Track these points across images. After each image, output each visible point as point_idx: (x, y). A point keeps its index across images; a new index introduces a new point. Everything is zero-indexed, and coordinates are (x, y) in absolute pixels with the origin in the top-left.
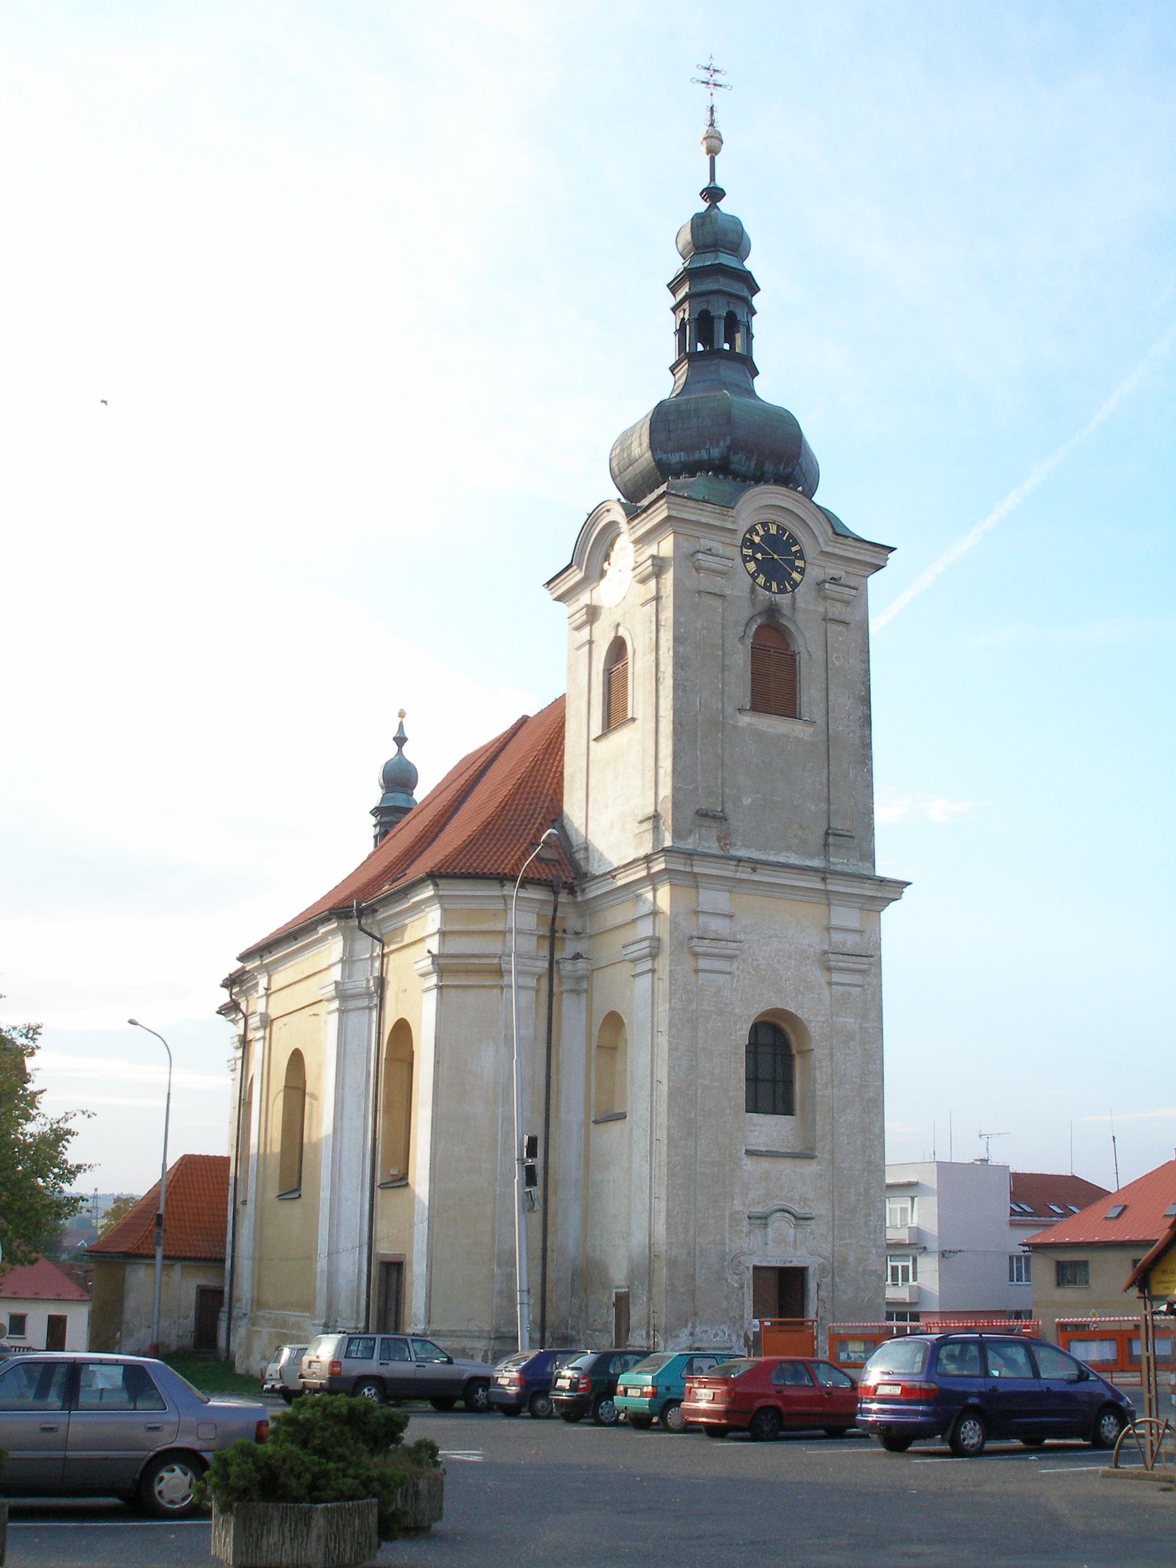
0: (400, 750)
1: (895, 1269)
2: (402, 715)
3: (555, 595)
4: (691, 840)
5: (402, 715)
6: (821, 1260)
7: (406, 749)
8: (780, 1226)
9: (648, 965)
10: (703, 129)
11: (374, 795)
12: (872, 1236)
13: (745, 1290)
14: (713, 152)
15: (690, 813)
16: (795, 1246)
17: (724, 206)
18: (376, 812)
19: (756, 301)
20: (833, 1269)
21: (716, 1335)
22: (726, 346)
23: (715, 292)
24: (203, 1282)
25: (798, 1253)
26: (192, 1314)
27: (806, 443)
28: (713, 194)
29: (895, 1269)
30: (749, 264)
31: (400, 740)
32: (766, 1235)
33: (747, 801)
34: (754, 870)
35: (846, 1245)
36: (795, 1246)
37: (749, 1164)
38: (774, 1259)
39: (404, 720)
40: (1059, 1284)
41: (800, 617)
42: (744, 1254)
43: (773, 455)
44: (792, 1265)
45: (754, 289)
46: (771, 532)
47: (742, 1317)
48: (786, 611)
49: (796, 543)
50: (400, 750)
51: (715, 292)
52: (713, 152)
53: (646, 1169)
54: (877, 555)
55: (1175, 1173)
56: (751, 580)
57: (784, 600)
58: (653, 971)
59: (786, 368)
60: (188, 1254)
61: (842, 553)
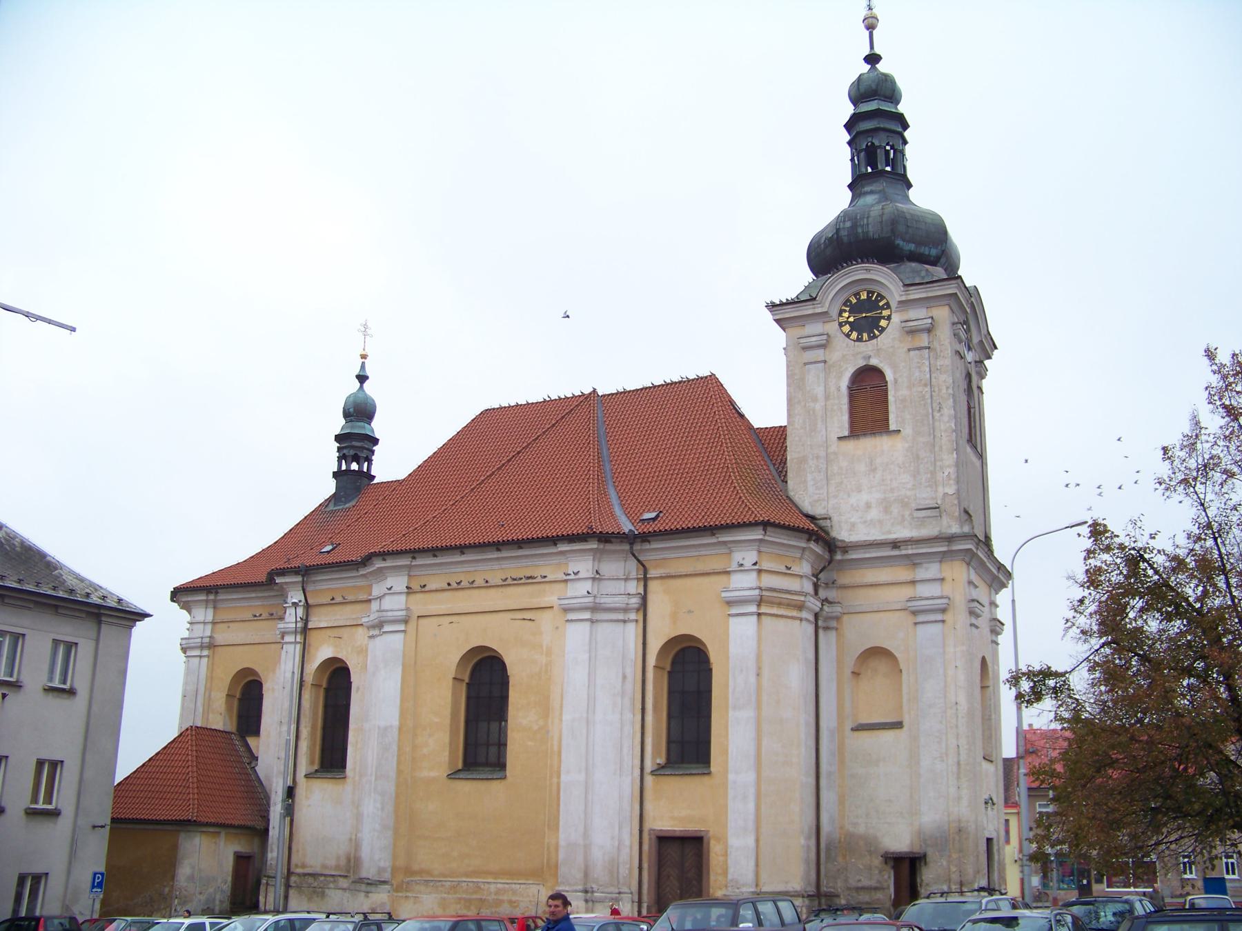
0: (361, 386)
2: (364, 357)
5: (364, 357)
7: (366, 385)
9: (402, 627)
10: (864, 12)
11: (338, 424)
14: (871, 28)
17: (881, 67)
18: (338, 438)
19: (907, 134)
22: (888, 169)
23: (876, 128)
26: (230, 879)
27: (952, 243)
28: (872, 59)
30: (901, 108)
31: (362, 378)
34: (414, 558)
43: (922, 249)
45: (905, 126)
50: (361, 386)
51: (876, 128)
52: (871, 28)
53: (750, 777)
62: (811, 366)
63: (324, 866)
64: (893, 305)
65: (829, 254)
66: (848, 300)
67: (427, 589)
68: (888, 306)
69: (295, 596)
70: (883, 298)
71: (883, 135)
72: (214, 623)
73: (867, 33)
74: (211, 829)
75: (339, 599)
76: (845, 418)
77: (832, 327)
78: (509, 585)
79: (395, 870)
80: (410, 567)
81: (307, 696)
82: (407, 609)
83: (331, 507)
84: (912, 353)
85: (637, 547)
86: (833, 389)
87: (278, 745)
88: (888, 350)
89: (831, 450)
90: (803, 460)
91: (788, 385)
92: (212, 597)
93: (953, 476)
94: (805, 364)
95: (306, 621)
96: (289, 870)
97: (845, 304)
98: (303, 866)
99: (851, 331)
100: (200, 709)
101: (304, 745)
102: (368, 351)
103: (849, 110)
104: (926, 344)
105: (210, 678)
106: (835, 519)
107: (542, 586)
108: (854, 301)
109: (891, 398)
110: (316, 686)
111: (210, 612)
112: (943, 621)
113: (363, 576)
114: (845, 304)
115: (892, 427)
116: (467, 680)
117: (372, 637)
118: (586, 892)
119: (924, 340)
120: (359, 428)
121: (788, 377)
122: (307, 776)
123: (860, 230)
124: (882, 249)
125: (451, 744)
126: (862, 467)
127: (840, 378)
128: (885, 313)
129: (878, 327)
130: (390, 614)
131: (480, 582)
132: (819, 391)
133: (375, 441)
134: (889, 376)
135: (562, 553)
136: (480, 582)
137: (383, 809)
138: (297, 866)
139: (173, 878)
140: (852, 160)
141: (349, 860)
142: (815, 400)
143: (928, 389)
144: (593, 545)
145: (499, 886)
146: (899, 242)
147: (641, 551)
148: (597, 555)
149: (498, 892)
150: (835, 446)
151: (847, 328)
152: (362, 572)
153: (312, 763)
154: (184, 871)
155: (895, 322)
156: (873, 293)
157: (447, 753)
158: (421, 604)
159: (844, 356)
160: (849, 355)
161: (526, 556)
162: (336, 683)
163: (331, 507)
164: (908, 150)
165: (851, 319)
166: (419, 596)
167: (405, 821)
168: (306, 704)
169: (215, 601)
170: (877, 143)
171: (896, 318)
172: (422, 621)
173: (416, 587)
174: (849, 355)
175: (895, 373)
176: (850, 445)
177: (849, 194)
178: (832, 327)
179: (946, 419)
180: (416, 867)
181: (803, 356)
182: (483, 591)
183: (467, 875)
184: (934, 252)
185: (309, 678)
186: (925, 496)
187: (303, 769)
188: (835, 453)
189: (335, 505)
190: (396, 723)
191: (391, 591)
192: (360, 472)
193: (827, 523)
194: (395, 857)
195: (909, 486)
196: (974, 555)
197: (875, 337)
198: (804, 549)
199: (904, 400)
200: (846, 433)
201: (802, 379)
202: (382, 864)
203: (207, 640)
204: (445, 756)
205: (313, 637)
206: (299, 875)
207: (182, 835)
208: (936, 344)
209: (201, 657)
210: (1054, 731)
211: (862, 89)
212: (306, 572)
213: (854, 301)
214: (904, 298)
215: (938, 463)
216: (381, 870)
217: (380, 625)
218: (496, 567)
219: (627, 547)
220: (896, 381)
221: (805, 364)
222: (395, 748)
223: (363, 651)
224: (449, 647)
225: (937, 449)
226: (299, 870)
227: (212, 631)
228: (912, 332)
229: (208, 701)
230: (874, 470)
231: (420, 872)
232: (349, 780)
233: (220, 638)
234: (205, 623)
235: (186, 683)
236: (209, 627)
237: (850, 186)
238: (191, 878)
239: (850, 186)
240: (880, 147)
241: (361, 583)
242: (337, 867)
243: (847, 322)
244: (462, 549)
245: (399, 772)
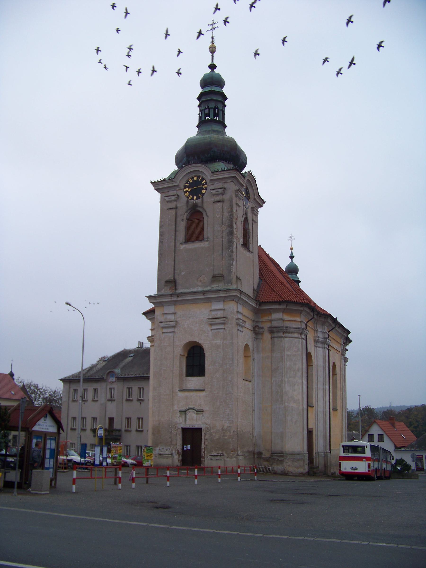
2: (292, 249)
3: (156, 188)
4: (163, 291)
5: (292, 249)
6: (206, 426)
8: (191, 415)
10: (210, 44)
12: (227, 417)
13: (178, 435)
15: (163, 282)
16: (197, 421)
17: (216, 71)
19: (226, 103)
20: (208, 429)
21: (167, 450)
23: (212, 97)
25: (198, 423)
28: (213, 67)
31: (292, 257)
32: (186, 417)
33: (183, 273)
35: (216, 420)
36: (197, 421)
37: (180, 394)
38: (189, 424)
40: (378, 435)
41: (205, 206)
42: (177, 424)
43: (234, 157)
44: (195, 427)
46: (195, 179)
47: (176, 444)
48: (200, 205)
49: (185, 186)
51: (212, 97)
54: (158, 186)
55: (425, 409)
56: (187, 199)
57: (199, 201)
59: (236, 128)
61: (217, 178)
64: (208, 182)
65: (190, 155)
68: (206, 183)
99: (189, 195)
102: (293, 247)
103: (200, 90)
108: (191, 181)
112: (224, 329)
128: (205, 187)
129: (201, 193)
140: (199, 114)
151: (187, 194)
164: (226, 110)
177: (197, 129)
196: (240, 298)
198: (302, 310)
210: (104, 366)
213: (191, 181)
237: (197, 126)
239: (197, 126)
243: (187, 191)
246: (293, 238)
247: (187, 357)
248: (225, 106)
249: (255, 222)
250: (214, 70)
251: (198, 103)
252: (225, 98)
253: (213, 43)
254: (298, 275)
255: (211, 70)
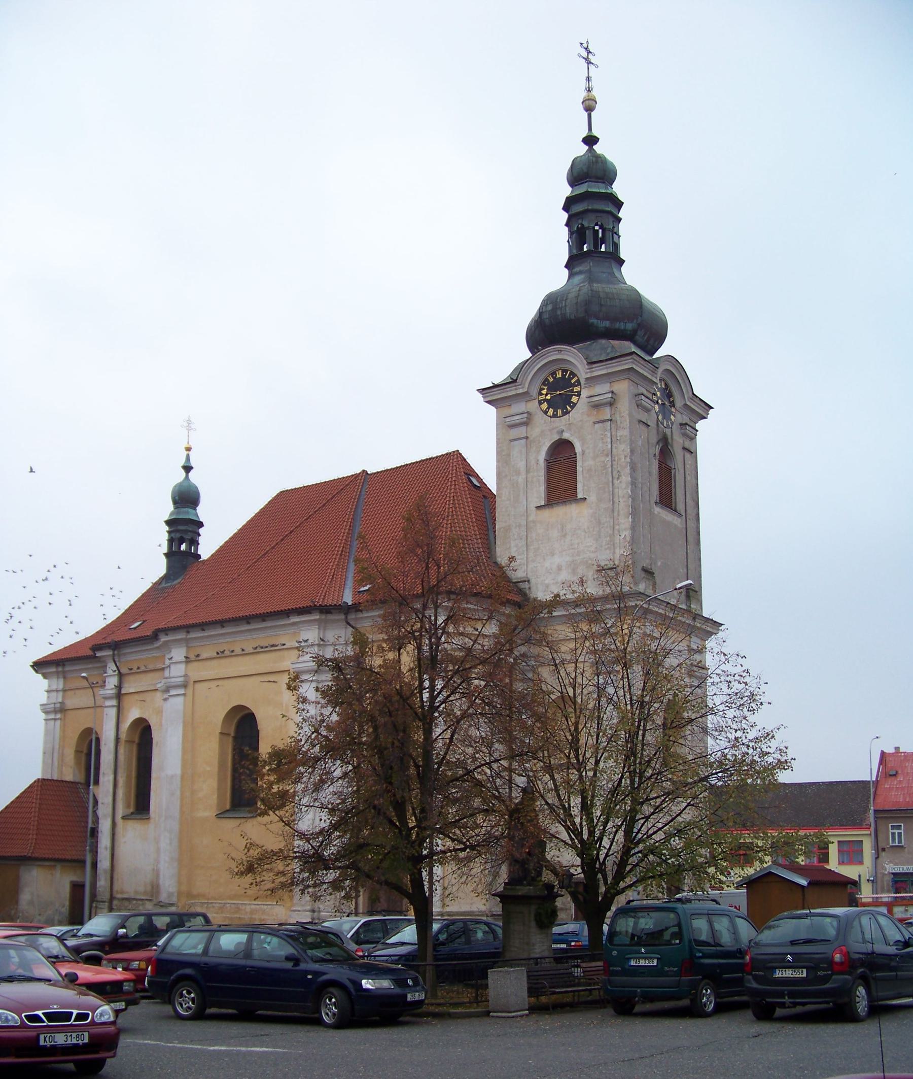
0: (187, 476)
1: (893, 834)
3: (488, 399)
7: (191, 474)
9: (182, 691)
10: (583, 94)
11: (167, 509)
18: (169, 523)
19: (621, 215)
23: (592, 205)
24: (75, 878)
26: (67, 903)
28: (590, 140)
29: (893, 834)
31: (188, 469)
34: (188, 632)
39: (190, 453)
43: (641, 328)
50: (187, 476)
51: (592, 205)
54: (493, 394)
58: (184, 695)
59: (646, 266)
60: (47, 856)
62: (516, 443)
63: (136, 892)
64: (582, 382)
65: (553, 328)
66: (547, 380)
67: (200, 658)
69: (111, 667)
70: (575, 375)
71: (592, 217)
72: (64, 691)
73: (586, 114)
74: (47, 863)
75: (143, 668)
76: (542, 489)
77: (533, 406)
78: (259, 652)
79: (180, 893)
80: (187, 641)
81: (121, 751)
82: (186, 676)
83: (163, 585)
84: (597, 426)
85: (352, 616)
86: (533, 462)
87: (109, 793)
88: (578, 425)
89: (531, 518)
90: (508, 529)
91: (498, 461)
92: (60, 669)
93: (628, 539)
94: (511, 441)
95: (119, 687)
96: (111, 895)
97: (544, 384)
98: (122, 892)
99: (548, 408)
100: (56, 763)
101: (120, 793)
102: (192, 445)
103: (567, 191)
104: (609, 417)
105: (63, 738)
106: (533, 581)
107: (281, 653)
108: (551, 380)
109: (579, 469)
110: (129, 742)
111: (61, 681)
113: (157, 648)
114: (544, 384)
115: (580, 496)
116: (233, 734)
117: (165, 700)
118: (313, 911)
119: (606, 413)
120: (188, 514)
121: (498, 453)
122: (124, 818)
123: (559, 312)
124: (595, 327)
125: (218, 789)
126: (555, 534)
127: (538, 452)
128: (576, 389)
129: (569, 402)
130: (173, 680)
131: (238, 651)
132: (522, 465)
133: (201, 525)
134: (578, 448)
135: (294, 624)
136: (238, 651)
137: (171, 844)
138: (117, 892)
139: (17, 902)
141: (153, 887)
142: (518, 473)
143: (609, 458)
144: (316, 616)
145: (253, 907)
146: (593, 321)
147: (356, 619)
148: (323, 625)
149: (252, 912)
150: (534, 515)
152: (157, 644)
153: (128, 806)
154: (25, 897)
155: (584, 397)
156: (566, 371)
157: (215, 797)
158: (198, 671)
159: (542, 432)
160: (546, 430)
161: (271, 627)
162: (143, 737)
163: (163, 585)
164: (622, 228)
165: (548, 397)
166: (195, 664)
167: (187, 856)
168: (121, 757)
169: (64, 672)
170: (586, 224)
171: (585, 393)
172: (198, 686)
173: (192, 657)
174: (546, 430)
175: (583, 445)
176: (546, 513)
177: (566, 271)
178: (533, 406)
179: (624, 485)
180: (195, 892)
181: (511, 430)
182: (240, 658)
183: (230, 898)
184: (630, 326)
185: (123, 736)
186: (604, 558)
187: (120, 812)
188: (534, 522)
189: (167, 582)
190: (179, 772)
191: (176, 660)
192: (187, 553)
193: (526, 585)
194: (180, 883)
195: (592, 549)
197: (568, 412)
199: (590, 470)
200: (543, 504)
201: (509, 455)
202: (171, 890)
203: (58, 705)
204: (214, 800)
205: (126, 701)
206: (118, 899)
207: (22, 868)
208: (617, 417)
209: (55, 719)
211: (575, 174)
212: (116, 646)
213: (551, 380)
214: (588, 376)
215: (617, 527)
216: (170, 895)
217: (167, 690)
218: (249, 637)
219: (342, 617)
220: (583, 453)
221: (511, 441)
222: (178, 793)
223: (159, 712)
224: (216, 707)
225: (616, 514)
226: (119, 896)
227: (63, 697)
228: (597, 406)
229: (62, 756)
230: (565, 536)
231: (198, 896)
232: (152, 821)
233: (70, 704)
234: (57, 691)
235: (45, 742)
236: (61, 694)
238: (31, 903)
240: (588, 228)
241: (156, 654)
242: (145, 893)
243: (545, 400)
244: (222, 623)
245: (182, 812)
246: (192, 426)
247: (235, 738)
248: (619, 220)
249: (691, 451)
250: (594, 147)
251: (565, 216)
252: (619, 204)
253: (589, 90)
254: (199, 509)
255: (587, 148)
